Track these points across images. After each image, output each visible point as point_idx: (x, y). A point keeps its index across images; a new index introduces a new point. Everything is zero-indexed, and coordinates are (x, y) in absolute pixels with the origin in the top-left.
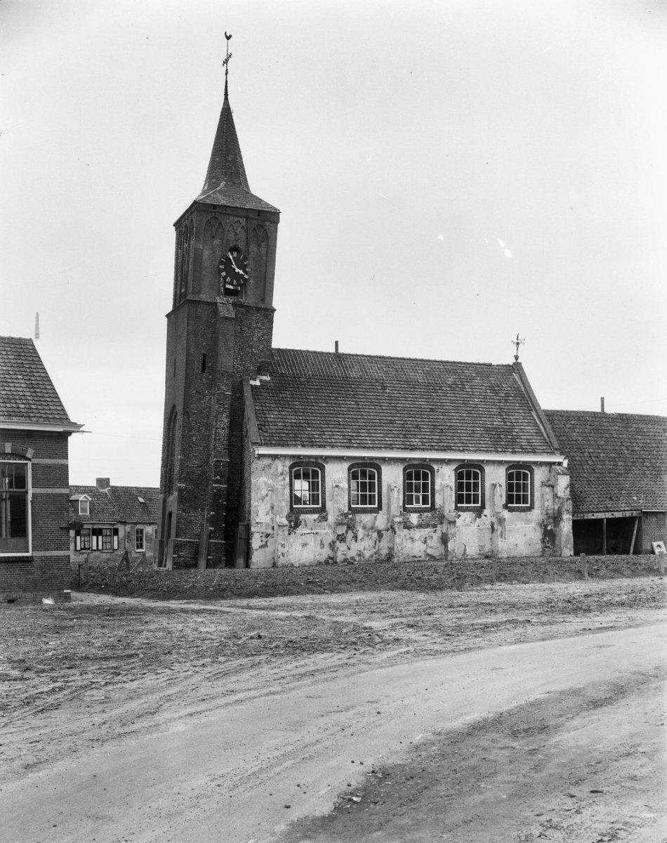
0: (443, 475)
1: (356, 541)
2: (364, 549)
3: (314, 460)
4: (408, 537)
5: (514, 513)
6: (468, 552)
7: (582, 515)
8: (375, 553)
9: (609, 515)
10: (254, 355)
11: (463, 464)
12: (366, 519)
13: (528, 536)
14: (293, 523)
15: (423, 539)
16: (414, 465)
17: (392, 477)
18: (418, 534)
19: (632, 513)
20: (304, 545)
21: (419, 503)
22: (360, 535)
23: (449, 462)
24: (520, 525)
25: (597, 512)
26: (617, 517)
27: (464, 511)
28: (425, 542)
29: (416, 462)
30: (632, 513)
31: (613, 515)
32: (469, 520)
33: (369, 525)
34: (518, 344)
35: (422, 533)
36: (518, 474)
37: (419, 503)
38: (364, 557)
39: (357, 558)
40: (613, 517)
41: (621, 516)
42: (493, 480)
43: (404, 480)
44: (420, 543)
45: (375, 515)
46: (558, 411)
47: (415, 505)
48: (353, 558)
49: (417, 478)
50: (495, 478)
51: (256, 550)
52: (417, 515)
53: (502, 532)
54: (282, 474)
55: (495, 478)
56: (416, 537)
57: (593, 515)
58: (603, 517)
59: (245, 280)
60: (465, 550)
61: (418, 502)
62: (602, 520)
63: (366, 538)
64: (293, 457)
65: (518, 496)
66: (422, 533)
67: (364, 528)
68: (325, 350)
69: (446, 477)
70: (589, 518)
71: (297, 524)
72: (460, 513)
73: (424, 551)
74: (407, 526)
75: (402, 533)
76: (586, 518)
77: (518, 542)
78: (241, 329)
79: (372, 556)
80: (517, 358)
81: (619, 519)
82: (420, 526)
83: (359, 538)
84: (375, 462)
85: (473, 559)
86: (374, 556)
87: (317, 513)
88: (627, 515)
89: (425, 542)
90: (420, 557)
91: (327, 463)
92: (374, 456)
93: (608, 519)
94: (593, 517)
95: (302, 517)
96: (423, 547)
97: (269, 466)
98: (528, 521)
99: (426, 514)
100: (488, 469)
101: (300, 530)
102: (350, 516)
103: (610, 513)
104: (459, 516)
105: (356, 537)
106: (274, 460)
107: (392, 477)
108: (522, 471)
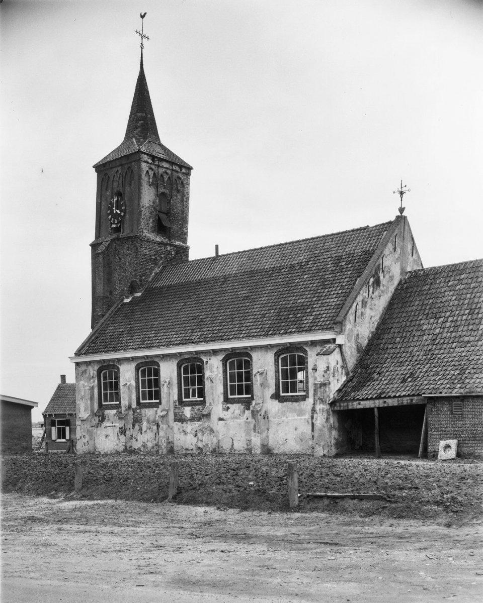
0: (211, 367)
1: (141, 433)
2: (148, 441)
3: (112, 363)
4: (181, 430)
5: (285, 403)
6: (236, 446)
7: (345, 404)
8: (156, 445)
9: (379, 403)
10: (126, 277)
11: (281, 350)
12: (149, 413)
13: (300, 431)
14: (100, 418)
15: (194, 432)
16: (186, 359)
17: (168, 372)
18: (190, 427)
19: (412, 400)
20: (107, 436)
21: (195, 397)
22: (144, 429)
23: (215, 352)
24: (292, 418)
25: (363, 399)
26: (390, 405)
27: (232, 404)
28: (196, 435)
29: (187, 356)
30: (412, 400)
31: (385, 402)
32: (237, 412)
33: (151, 419)
34: (402, 193)
35: (193, 427)
36: (193, 367)
37: (195, 397)
38: (147, 448)
39: (142, 449)
40: (385, 405)
41: (396, 404)
42: (261, 367)
43: (160, 378)
44: (192, 436)
45: (155, 409)
46: (448, 266)
47: (191, 399)
48: (139, 449)
49: (193, 372)
50: (264, 365)
51: (78, 440)
52: (190, 408)
53: (255, 426)
54: (93, 377)
55: (264, 365)
56: (188, 430)
57: (359, 404)
58: (372, 406)
59: (122, 217)
60: (233, 445)
61: (194, 396)
62: (372, 409)
63: (148, 431)
64: (99, 362)
65: (240, 386)
66: (193, 427)
67: (148, 421)
68: (190, 254)
69: (215, 369)
70: (355, 407)
71: (103, 419)
72: (228, 405)
73: (196, 444)
74: (180, 419)
75: (177, 426)
76: (350, 407)
77: (289, 437)
78: (119, 258)
79: (153, 448)
80: (402, 210)
81: (393, 407)
82: (193, 419)
83: (144, 430)
84: (155, 360)
85: (241, 455)
86: (155, 448)
87: (189, 406)
88: (405, 403)
89: (196, 435)
90: (192, 450)
91: (120, 365)
92: (223, 348)
93: (379, 408)
94: (359, 407)
95: (107, 412)
96: (194, 440)
97: (85, 371)
98: (301, 413)
99: (197, 407)
100: (255, 356)
101: (106, 423)
102: (138, 411)
103: (381, 401)
104: (228, 408)
105: (142, 430)
106: (87, 366)
107: (168, 372)
108: (297, 354)
